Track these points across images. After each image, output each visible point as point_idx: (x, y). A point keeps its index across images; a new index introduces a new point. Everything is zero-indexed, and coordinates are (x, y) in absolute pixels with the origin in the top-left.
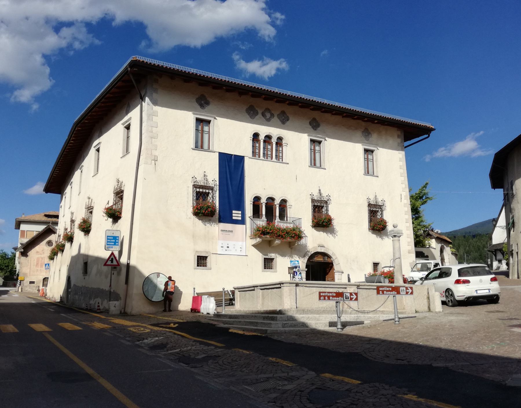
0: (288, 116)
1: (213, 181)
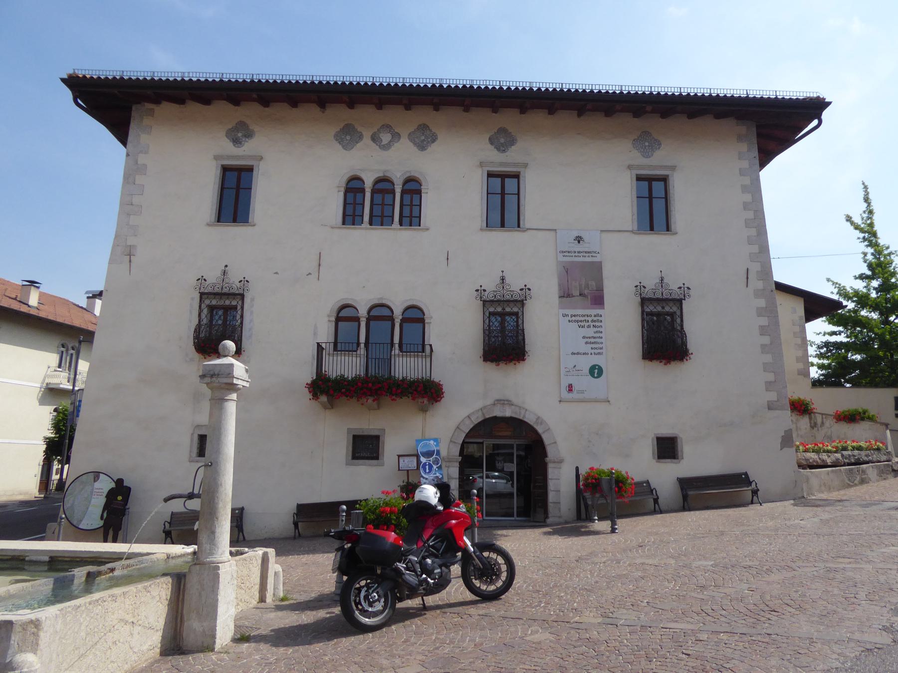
0: (435, 133)
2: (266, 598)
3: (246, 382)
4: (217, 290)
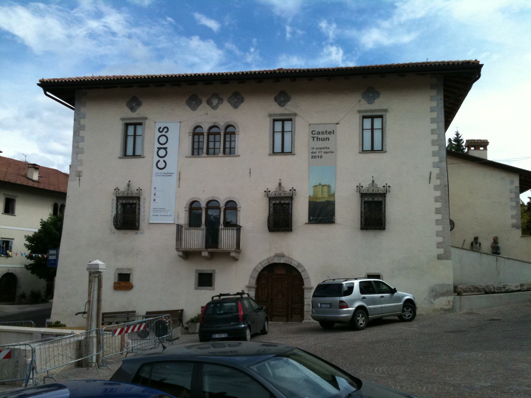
0: (243, 97)
1: (137, 190)
4: (125, 195)
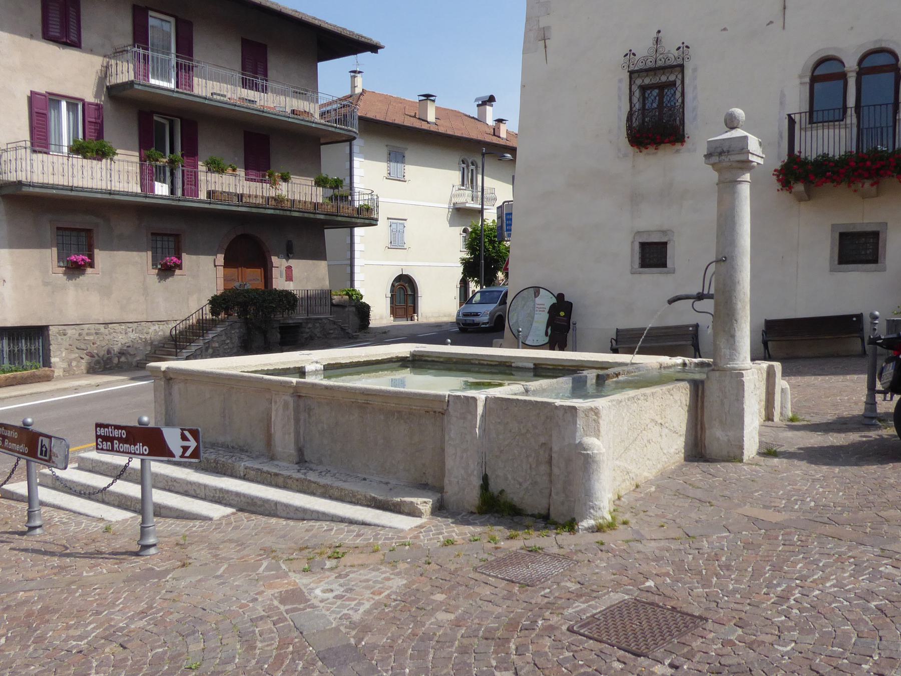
1: (679, 48)
2: (773, 416)
3: (760, 158)
4: (649, 65)
